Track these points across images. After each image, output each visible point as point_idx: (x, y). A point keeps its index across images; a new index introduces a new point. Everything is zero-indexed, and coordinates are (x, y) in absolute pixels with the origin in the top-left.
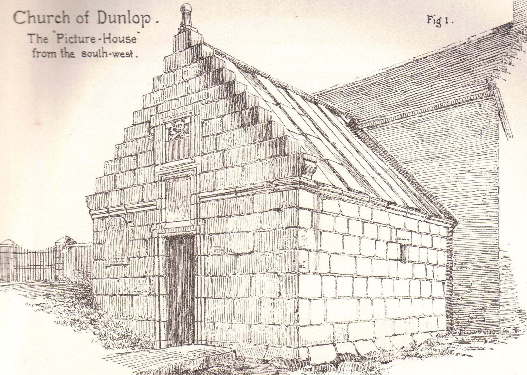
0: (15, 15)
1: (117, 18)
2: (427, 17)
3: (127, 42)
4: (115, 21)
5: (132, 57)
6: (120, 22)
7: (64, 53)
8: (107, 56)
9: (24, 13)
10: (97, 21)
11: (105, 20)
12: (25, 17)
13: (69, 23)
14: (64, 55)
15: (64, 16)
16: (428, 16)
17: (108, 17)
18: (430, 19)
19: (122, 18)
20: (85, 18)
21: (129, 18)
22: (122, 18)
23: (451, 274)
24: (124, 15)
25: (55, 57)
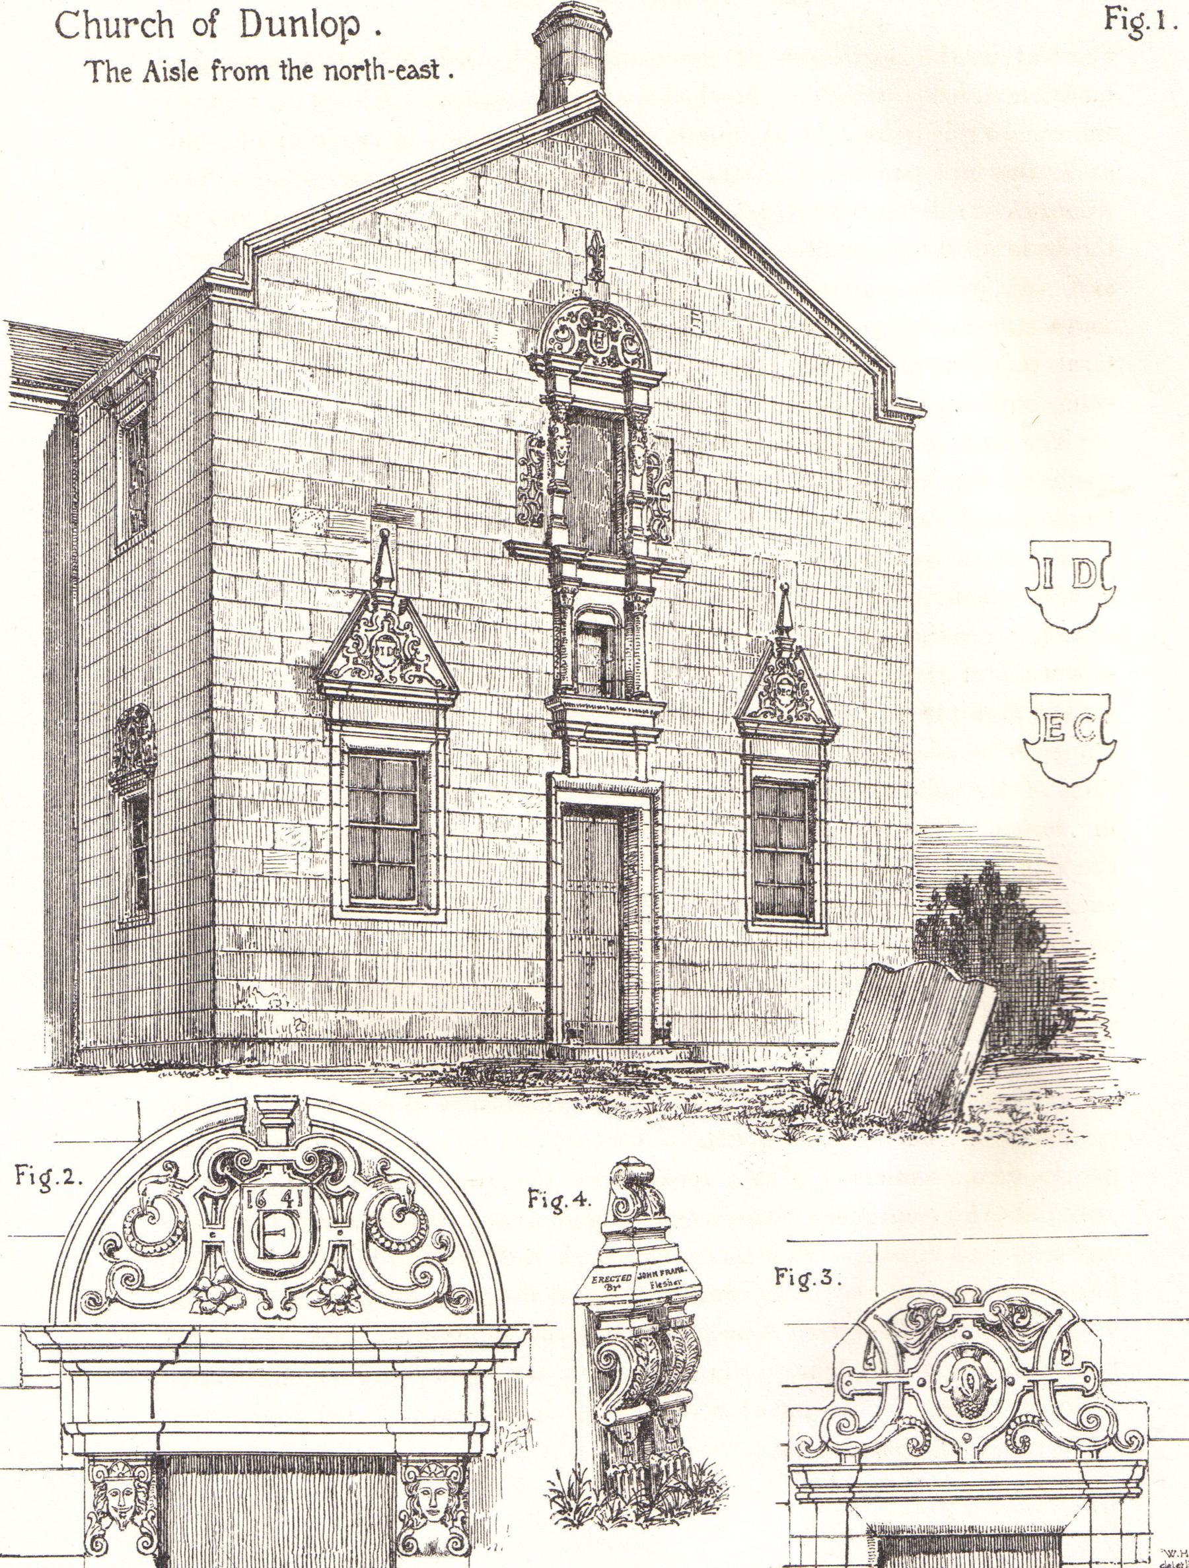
0: (198, 20)
1: (288, 23)
2: (775, 1271)
3: (172, 78)
4: (282, 32)
5: (436, 77)
6: (294, 34)
7: (287, 70)
8: (383, 77)
9: (76, 14)
10: (241, 32)
11: (205, 32)
12: (78, 24)
13: (171, 36)
14: (288, 75)
15: (161, 22)
16: (778, 1269)
17: (265, 24)
18: (536, 1198)
19: (299, 26)
20: (210, 25)
21: (315, 23)
22: (299, 26)
23: (140, 361)
24: (303, 18)
25: (266, 78)
